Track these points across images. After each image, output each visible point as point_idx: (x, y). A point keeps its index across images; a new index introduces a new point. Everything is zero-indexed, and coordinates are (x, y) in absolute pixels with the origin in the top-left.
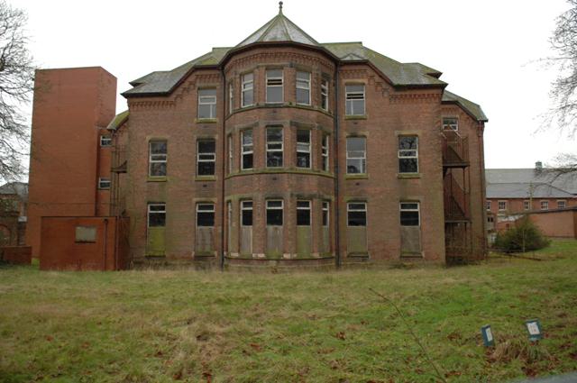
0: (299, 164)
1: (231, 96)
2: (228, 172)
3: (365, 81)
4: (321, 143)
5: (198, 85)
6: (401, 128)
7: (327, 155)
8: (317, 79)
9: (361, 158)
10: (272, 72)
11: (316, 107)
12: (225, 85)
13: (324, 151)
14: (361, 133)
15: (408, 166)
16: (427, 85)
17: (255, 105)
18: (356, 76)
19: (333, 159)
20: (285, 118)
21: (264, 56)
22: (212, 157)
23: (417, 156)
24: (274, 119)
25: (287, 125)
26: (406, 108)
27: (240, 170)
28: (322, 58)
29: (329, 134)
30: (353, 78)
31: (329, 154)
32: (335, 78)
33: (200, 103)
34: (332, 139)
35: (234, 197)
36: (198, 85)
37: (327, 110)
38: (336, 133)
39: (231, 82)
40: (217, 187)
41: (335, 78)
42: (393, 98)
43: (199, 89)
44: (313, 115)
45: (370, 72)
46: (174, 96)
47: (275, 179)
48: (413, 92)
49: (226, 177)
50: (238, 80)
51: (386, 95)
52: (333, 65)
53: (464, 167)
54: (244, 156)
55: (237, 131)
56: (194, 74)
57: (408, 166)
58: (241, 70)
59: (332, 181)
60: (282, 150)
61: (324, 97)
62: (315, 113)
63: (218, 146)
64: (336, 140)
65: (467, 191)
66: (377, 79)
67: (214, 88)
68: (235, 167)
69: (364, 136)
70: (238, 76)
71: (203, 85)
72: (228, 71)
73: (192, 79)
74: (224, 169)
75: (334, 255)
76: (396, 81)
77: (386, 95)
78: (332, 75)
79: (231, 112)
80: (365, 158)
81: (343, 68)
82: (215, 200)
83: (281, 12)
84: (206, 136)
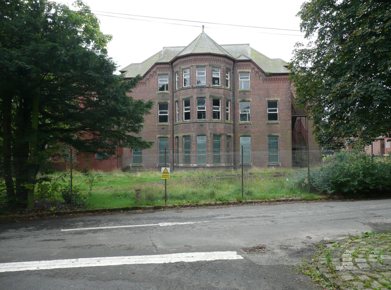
0: (214, 83)
1: (177, 80)
2: (176, 121)
3: (250, 71)
4: (225, 106)
5: (158, 73)
6: (269, 97)
7: (229, 112)
8: (223, 71)
9: (248, 113)
10: (200, 68)
11: (223, 87)
12: (173, 73)
13: (227, 110)
14: (247, 99)
15: (273, 117)
16: (284, 73)
17: (191, 86)
18: (245, 67)
19: (232, 114)
20: (207, 94)
21: (195, 60)
22: (167, 113)
23: (277, 112)
24: (201, 94)
25: (208, 97)
26: (272, 86)
27: (183, 121)
28: (226, 60)
29: (230, 101)
30: (243, 69)
31: (230, 111)
32: (233, 69)
33: (159, 83)
34: (232, 103)
35: (180, 135)
36: (158, 73)
37: (229, 88)
38: (234, 99)
39: (177, 72)
40: (170, 129)
41: (233, 69)
42: (265, 80)
43: (158, 75)
44: (222, 91)
45: (252, 66)
46: (145, 79)
47: (202, 125)
48: (276, 77)
49: (175, 123)
50: (181, 72)
51: (261, 78)
52: (232, 62)
53: (306, 117)
54: (185, 113)
55: (181, 99)
56: (156, 67)
57: (273, 117)
58: (183, 67)
59: (232, 126)
60: (205, 110)
61: (227, 81)
62: (223, 90)
63: (170, 107)
64: (234, 103)
65: (307, 130)
66: (256, 69)
67: (167, 74)
68: (180, 119)
69: (249, 101)
70: (181, 70)
71: (160, 73)
72: (175, 66)
73: (154, 69)
74: (173, 120)
75: (232, 165)
76: (267, 70)
77: (261, 78)
78: (232, 68)
79: (177, 89)
80: (250, 113)
81: (237, 64)
82: (169, 136)
83: (203, 31)
84: (163, 101)
